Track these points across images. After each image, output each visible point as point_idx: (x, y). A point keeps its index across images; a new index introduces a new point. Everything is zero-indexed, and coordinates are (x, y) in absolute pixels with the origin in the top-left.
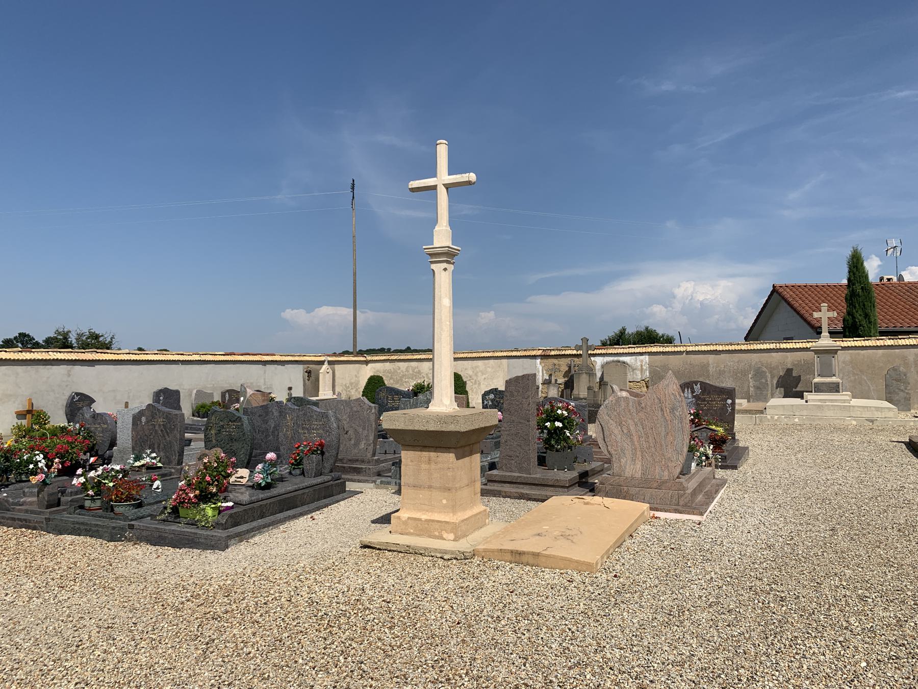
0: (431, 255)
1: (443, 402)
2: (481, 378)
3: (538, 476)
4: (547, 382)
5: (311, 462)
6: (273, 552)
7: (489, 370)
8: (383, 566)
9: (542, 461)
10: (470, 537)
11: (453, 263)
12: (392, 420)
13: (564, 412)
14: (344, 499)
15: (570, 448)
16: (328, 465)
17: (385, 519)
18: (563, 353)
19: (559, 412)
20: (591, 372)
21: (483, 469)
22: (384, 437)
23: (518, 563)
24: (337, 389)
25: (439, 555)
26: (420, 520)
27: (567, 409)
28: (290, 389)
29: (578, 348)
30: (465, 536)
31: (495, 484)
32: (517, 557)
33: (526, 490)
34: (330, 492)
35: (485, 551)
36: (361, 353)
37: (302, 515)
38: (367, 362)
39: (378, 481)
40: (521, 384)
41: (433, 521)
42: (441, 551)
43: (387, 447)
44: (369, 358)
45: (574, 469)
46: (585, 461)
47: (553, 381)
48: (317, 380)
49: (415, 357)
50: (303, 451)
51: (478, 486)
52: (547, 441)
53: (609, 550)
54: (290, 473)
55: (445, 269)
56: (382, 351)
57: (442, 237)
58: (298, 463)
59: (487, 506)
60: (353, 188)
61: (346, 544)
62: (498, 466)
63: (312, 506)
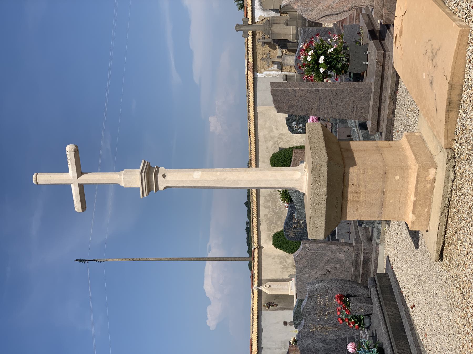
0: (150, 189)
1: (298, 178)
2: (276, 133)
3: (373, 81)
4: (281, 66)
5: (358, 308)
6: (446, 347)
7: (268, 124)
8: (460, 240)
9: (359, 77)
10: (433, 152)
11: (158, 168)
12: (316, 228)
13: (310, 54)
14: (395, 276)
15: (345, 48)
16: (361, 291)
17: (415, 236)
18: (250, 49)
19: (309, 59)
20: (270, 22)
21: (367, 138)
22: (334, 233)
23: (459, 105)
24: (287, 277)
25: (451, 184)
26: (415, 203)
27: (307, 51)
28: (285, 323)
29: (246, 35)
30: (431, 157)
31: (380, 126)
32: (453, 105)
33: (387, 94)
34: (387, 287)
35: (446, 137)
36: (250, 252)
37: (409, 317)
38: (260, 248)
39: (377, 240)
40: (281, 97)
41: (416, 189)
42: (447, 182)
43: (343, 232)
44: (255, 245)
45: (367, 45)
46: (359, 33)
47: (279, 60)
48: (277, 296)
49: (255, 199)
50: (346, 316)
51: (383, 143)
52: (339, 72)
53: (447, 13)
54: (368, 328)
55: (164, 176)
56: (249, 231)
57: (131, 179)
58: (358, 320)
59: (402, 133)
60: (84, 261)
61: (439, 276)
62: (363, 121)
63: (401, 307)
